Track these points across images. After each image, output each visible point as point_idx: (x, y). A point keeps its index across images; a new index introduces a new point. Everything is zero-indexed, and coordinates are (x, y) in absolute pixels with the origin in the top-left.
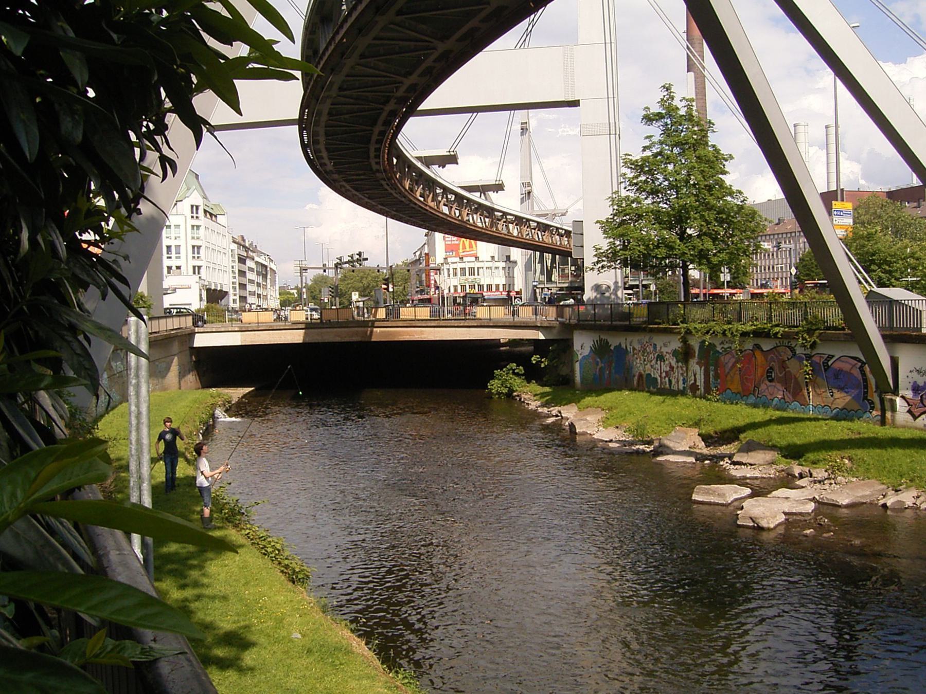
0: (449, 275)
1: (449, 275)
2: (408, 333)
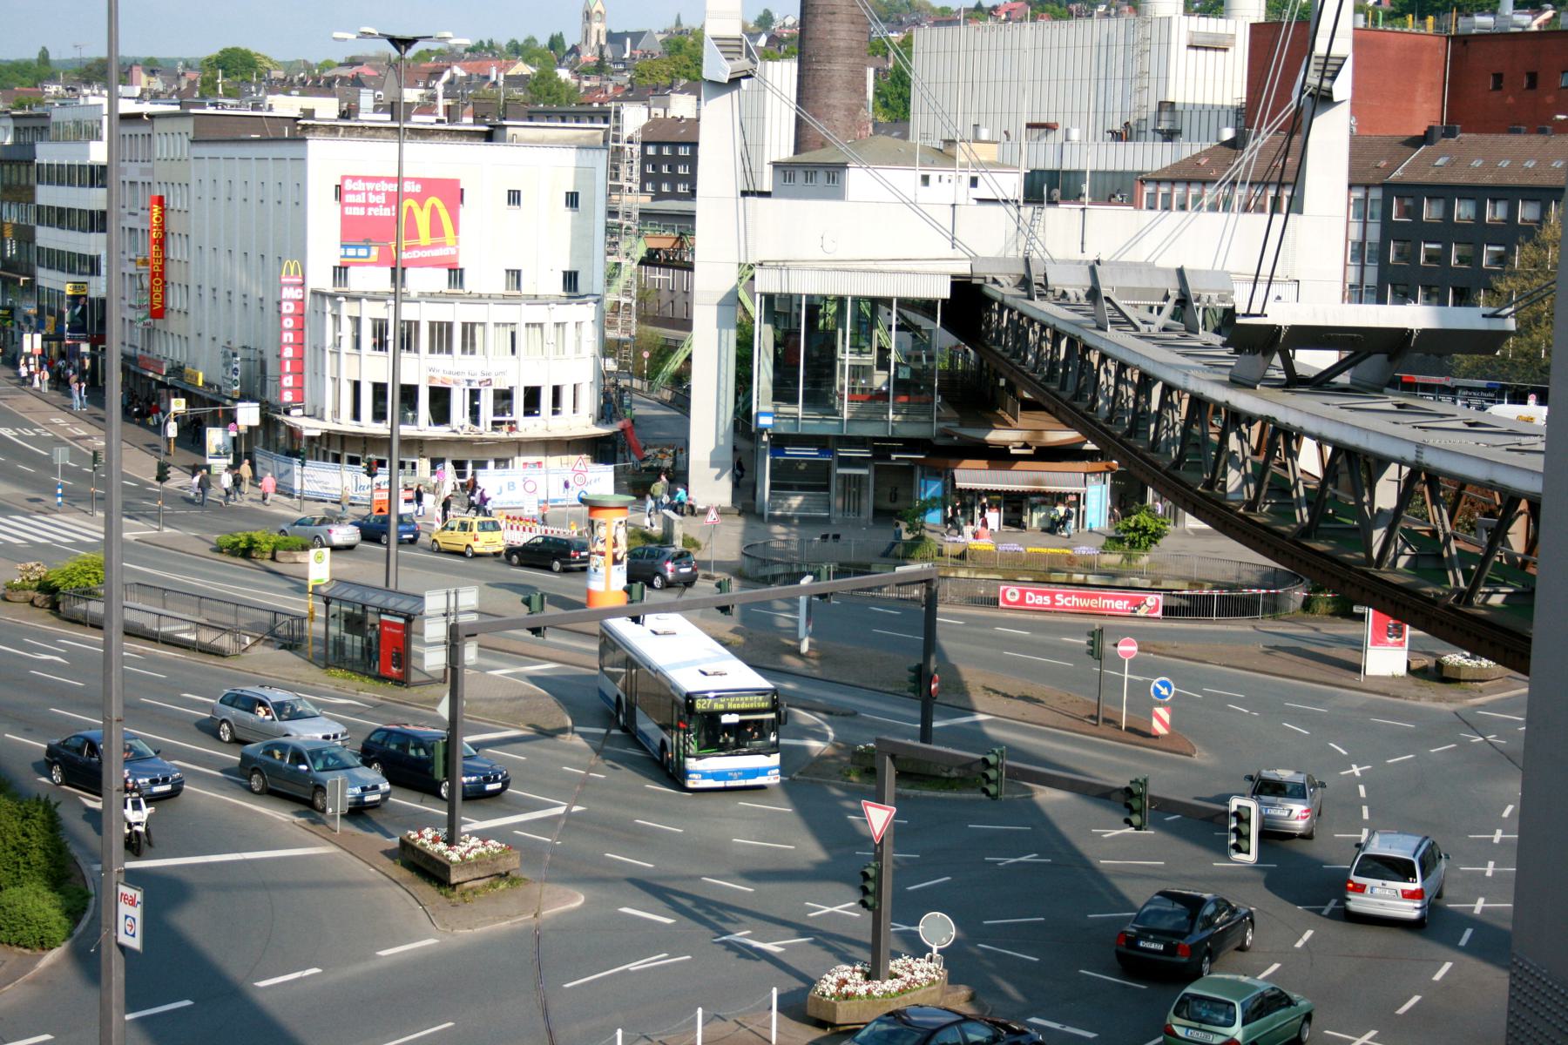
0: (556, 391)
1: (556, 391)
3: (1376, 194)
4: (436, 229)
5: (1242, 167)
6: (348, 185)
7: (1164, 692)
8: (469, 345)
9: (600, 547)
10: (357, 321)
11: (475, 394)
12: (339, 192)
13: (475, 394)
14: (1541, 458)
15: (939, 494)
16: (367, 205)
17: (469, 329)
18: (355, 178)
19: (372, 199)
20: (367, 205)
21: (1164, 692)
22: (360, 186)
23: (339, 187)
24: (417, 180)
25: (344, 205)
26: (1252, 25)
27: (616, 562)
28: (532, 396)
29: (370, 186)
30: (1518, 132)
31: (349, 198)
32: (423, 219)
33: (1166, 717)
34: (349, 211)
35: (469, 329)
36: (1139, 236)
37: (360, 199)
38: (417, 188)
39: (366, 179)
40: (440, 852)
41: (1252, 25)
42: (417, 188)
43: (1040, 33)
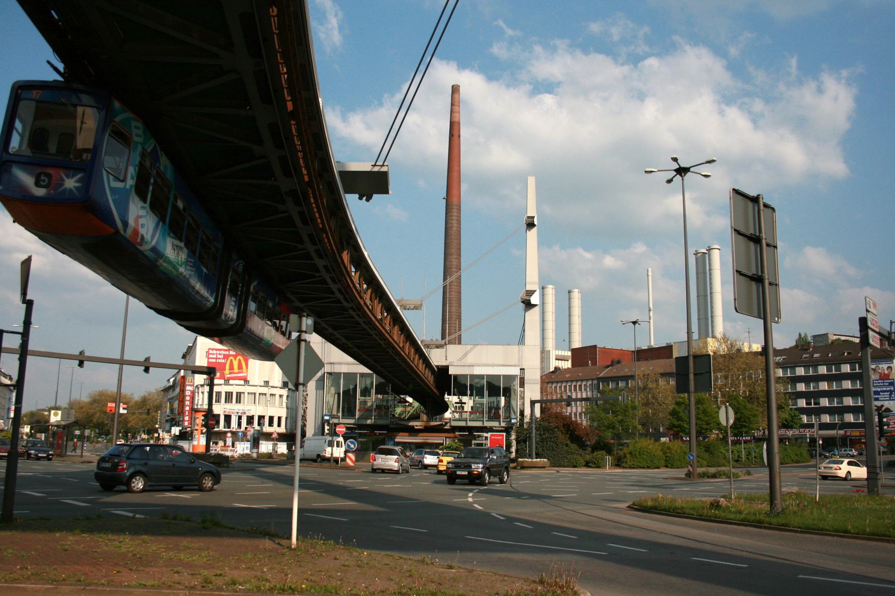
0: (279, 418)
1: (279, 418)
3: (595, 382)
4: (240, 367)
7: (352, 446)
8: (239, 401)
9: (196, 427)
11: (240, 418)
12: (208, 353)
13: (240, 418)
16: (216, 358)
17: (239, 395)
18: (213, 349)
21: (352, 446)
22: (215, 352)
23: (208, 352)
25: (209, 358)
26: (387, 192)
27: (202, 433)
28: (271, 419)
32: (236, 364)
33: (353, 458)
35: (239, 395)
36: (466, 355)
37: (214, 356)
41: (387, 192)
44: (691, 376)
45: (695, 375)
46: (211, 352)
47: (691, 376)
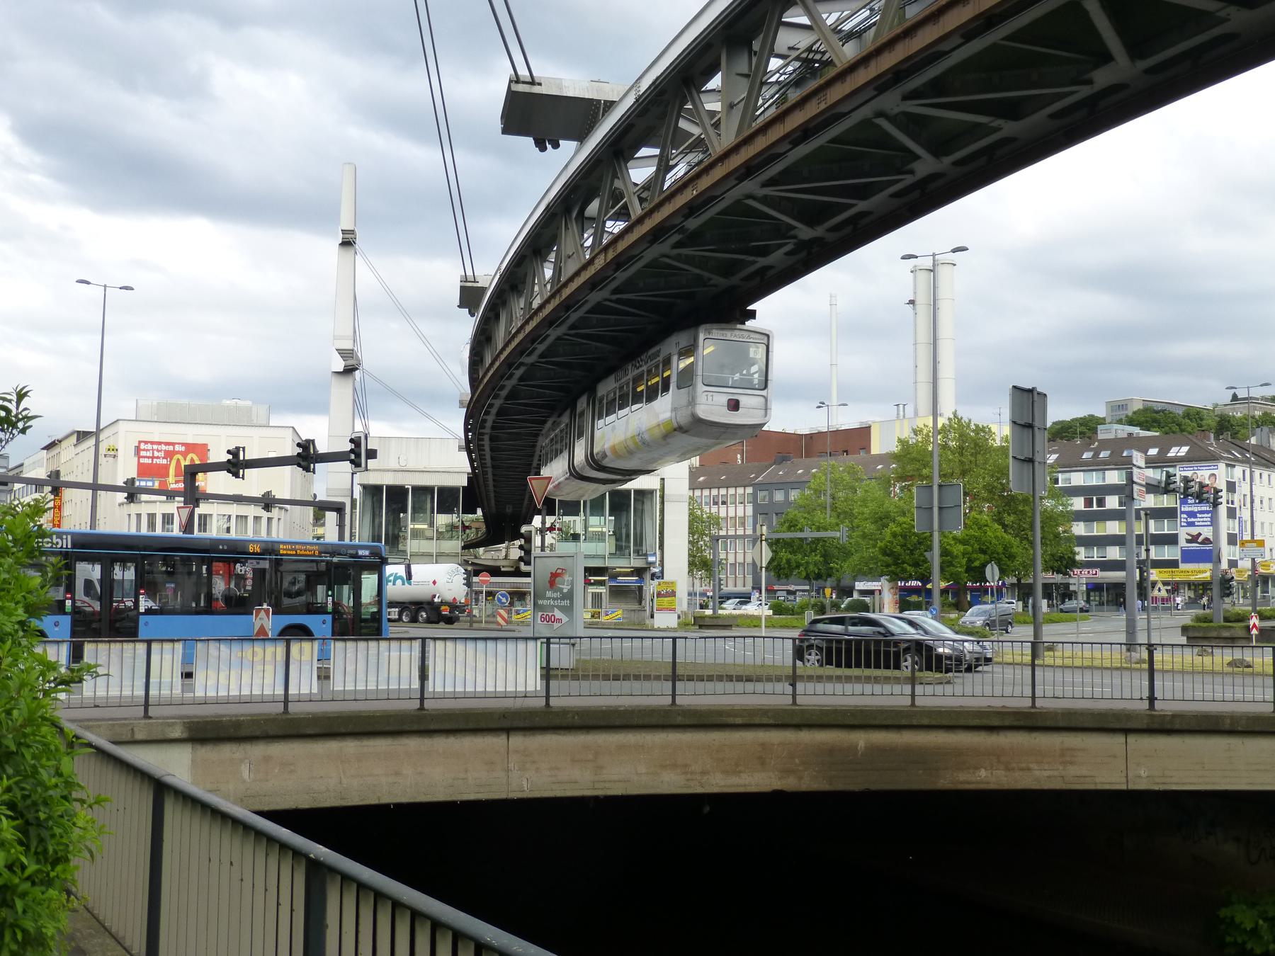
2: (1066, 756)
5: (488, 360)
6: (142, 446)
10: (139, 516)
12: (138, 450)
14: (225, 694)
15: (764, 89)
16: (153, 458)
18: (146, 443)
19: (156, 454)
20: (153, 458)
22: (149, 446)
24: (183, 444)
25: (139, 457)
29: (155, 447)
30: (466, 431)
31: (142, 453)
34: (142, 461)
37: (149, 454)
38: (183, 449)
39: (152, 443)
40: (558, 285)
42: (183, 449)
43: (394, 654)
44: (936, 510)
45: (940, 508)
46: (142, 446)
47: (936, 510)
